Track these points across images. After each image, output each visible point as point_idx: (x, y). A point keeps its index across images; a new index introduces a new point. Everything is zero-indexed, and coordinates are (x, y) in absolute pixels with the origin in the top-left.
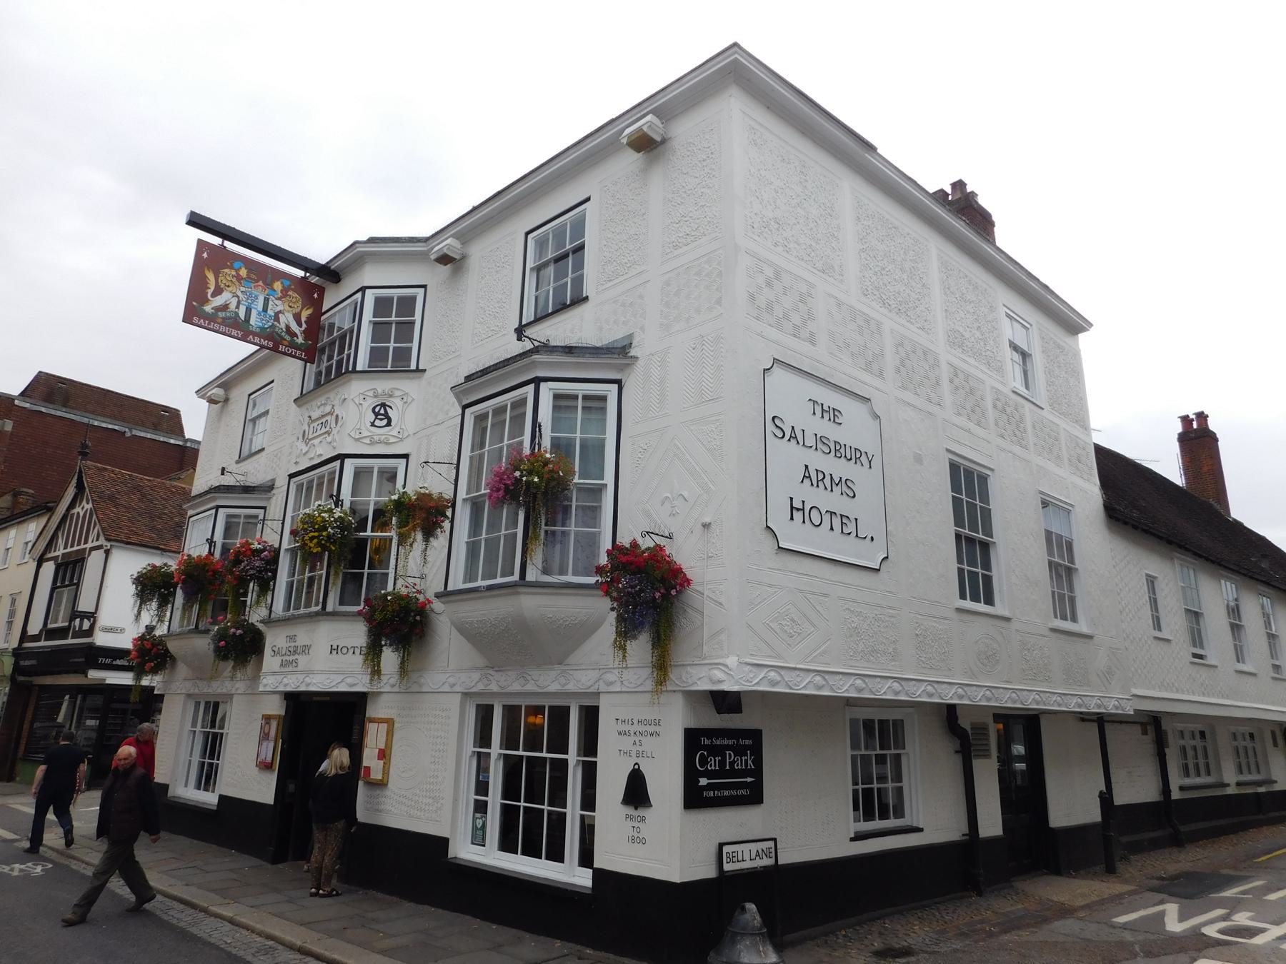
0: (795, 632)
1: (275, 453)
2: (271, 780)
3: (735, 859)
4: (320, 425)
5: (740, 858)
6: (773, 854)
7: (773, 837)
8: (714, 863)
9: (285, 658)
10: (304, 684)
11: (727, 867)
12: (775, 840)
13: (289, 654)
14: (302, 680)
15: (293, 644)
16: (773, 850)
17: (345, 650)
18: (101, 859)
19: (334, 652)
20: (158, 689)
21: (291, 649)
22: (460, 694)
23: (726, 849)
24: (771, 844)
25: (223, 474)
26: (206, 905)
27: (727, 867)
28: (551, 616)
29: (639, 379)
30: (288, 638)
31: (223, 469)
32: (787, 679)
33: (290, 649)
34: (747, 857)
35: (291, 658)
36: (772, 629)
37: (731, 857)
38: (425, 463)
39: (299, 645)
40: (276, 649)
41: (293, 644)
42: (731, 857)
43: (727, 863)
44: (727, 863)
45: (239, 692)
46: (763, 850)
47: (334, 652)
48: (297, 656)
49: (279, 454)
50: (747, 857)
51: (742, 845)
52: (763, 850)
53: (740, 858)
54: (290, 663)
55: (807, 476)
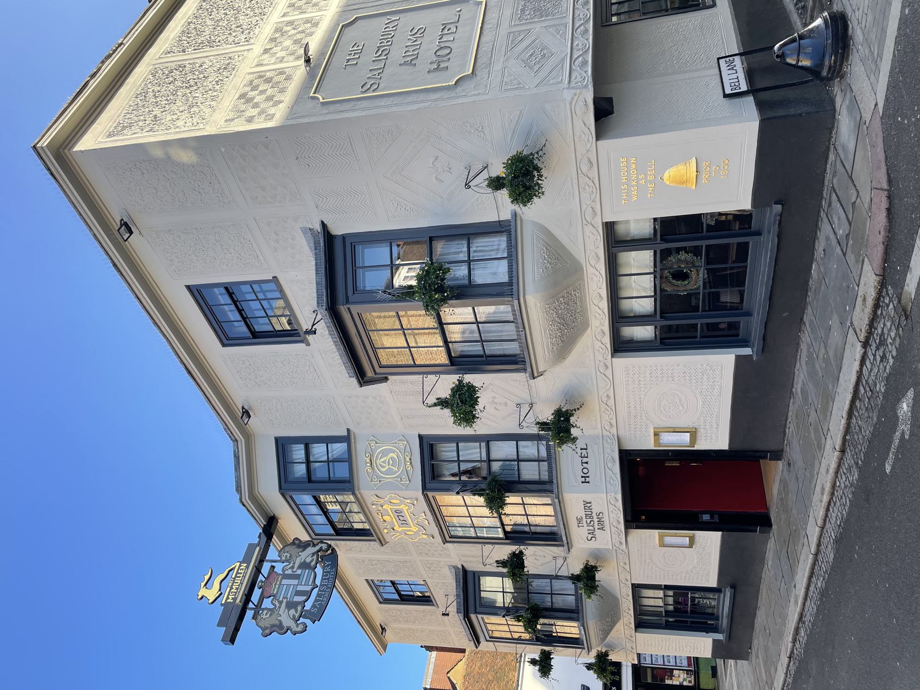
0: (541, 53)
1: (427, 569)
2: (702, 536)
3: (737, 84)
4: (400, 517)
5: (737, 80)
6: (731, 58)
7: (716, 60)
8: (741, 99)
9: (596, 527)
10: (616, 505)
11: (744, 87)
12: (718, 59)
13: (592, 522)
14: (616, 528)
15: (584, 520)
16: (727, 59)
17: (585, 471)
18: (742, 97)
19: (588, 479)
20: (634, 660)
21: (589, 521)
22: (613, 359)
23: (728, 91)
24: (722, 62)
25: (448, 615)
26: (811, 556)
27: (744, 87)
28: (541, 270)
29: (343, 217)
30: (580, 525)
31: (444, 614)
32: (581, 53)
33: (588, 522)
34: (735, 76)
35: (596, 520)
36: (539, 69)
37: (735, 87)
38: (423, 403)
39: (584, 513)
40: (590, 536)
41: (584, 520)
42: (735, 87)
43: (740, 89)
44: (740, 89)
45: (629, 578)
46: (728, 66)
47: (588, 479)
48: (594, 515)
49: (428, 565)
50: (735, 76)
51: (724, 82)
52: (728, 66)
53: (737, 80)
54: (600, 522)
55: (411, 63)
